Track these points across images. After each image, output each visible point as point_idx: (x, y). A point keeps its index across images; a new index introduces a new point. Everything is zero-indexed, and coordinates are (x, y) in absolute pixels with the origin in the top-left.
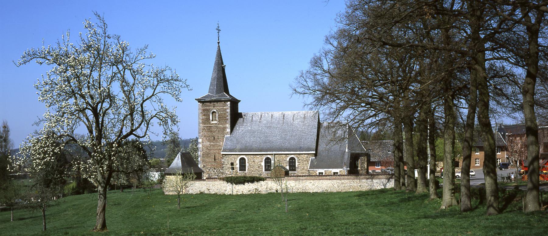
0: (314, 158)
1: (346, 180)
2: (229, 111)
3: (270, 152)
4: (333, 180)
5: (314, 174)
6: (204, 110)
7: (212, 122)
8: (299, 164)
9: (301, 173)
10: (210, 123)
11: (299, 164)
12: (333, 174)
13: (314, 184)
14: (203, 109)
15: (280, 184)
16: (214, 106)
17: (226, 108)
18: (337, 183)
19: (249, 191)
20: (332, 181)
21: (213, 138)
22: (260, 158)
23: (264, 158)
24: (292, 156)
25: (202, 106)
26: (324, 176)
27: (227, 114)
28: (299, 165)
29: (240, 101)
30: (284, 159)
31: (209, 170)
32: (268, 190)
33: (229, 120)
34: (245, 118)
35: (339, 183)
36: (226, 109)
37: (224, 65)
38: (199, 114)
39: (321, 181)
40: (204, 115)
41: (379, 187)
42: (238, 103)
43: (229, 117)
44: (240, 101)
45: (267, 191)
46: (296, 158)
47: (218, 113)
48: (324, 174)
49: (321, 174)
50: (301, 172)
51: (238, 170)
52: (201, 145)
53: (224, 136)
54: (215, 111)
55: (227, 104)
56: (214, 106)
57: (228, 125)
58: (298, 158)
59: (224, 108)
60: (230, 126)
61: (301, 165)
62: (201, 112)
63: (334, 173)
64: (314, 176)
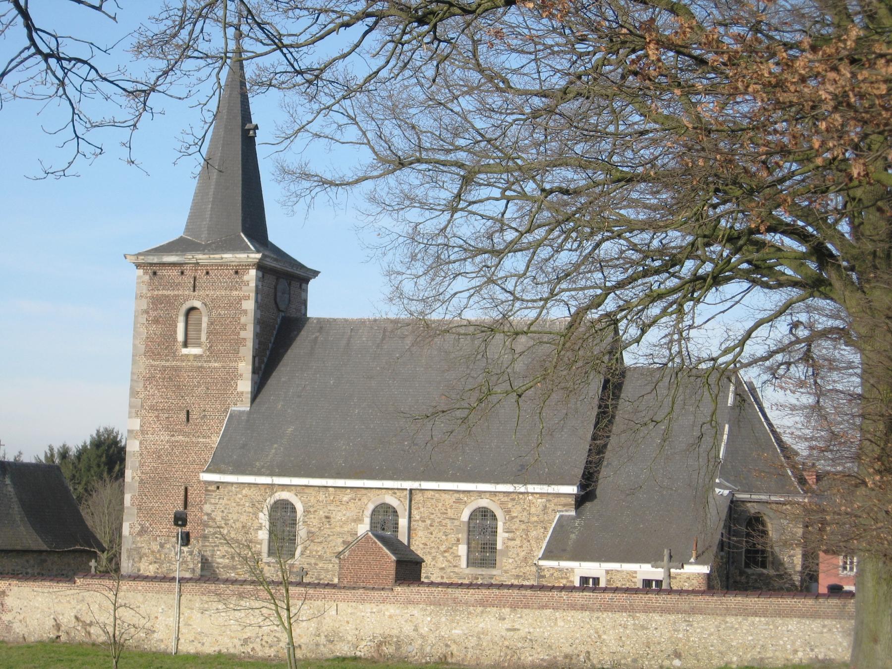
0: (573, 513)
1: (656, 617)
2: (249, 305)
3: (321, 476)
4: (599, 610)
5: (563, 582)
6: (156, 302)
7: (185, 351)
8: (511, 535)
9: (518, 577)
10: (174, 355)
11: (511, 535)
12: (640, 585)
13: (517, 626)
14: (152, 297)
15: (284, 614)
16: (194, 287)
17: (241, 294)
18: (614, 627)
19: (246, 641)
20: (596, 614)
21: (183, 416)
22: (351, 505)
23: (371, 507)
24: (484, 503)
25: (152, 286)
26: (605, 590)
27: (243, 320)
28: (511, 543)
29: (315, 273)
30: (450, 513)
31: (162, 546)
32: (322, 640)
33: (250, 344)
34: (321, 339)
35: (625, 627)
36: (240, 300)
37: (254, 122)
38: (136, 317)
39: (548, 612)
40: (156, 321)
41: (800, 654)
42: (307, 281)
43: (248, 334)
44: (315, 273)
45: (317, 645)
46: (499, 514)
47: (209, 316)
48: (602, 584)
49: (588, 584)
50: (514, 572)
51: (463, 563)
52: (137, 443)
53: (226, 411)
54: (197, 304)
55: (246, 278)
56: (194, 287)
57: (245, 367)
58: (508, 512)
59: (235, 293)
60: (250, 367)
61: (518, 542)
62: (145, 307)
63: (584, 580)
64: (563, 588)
